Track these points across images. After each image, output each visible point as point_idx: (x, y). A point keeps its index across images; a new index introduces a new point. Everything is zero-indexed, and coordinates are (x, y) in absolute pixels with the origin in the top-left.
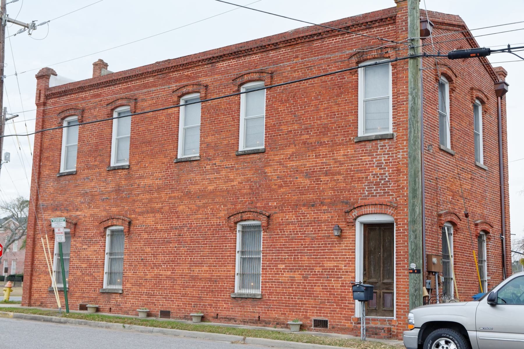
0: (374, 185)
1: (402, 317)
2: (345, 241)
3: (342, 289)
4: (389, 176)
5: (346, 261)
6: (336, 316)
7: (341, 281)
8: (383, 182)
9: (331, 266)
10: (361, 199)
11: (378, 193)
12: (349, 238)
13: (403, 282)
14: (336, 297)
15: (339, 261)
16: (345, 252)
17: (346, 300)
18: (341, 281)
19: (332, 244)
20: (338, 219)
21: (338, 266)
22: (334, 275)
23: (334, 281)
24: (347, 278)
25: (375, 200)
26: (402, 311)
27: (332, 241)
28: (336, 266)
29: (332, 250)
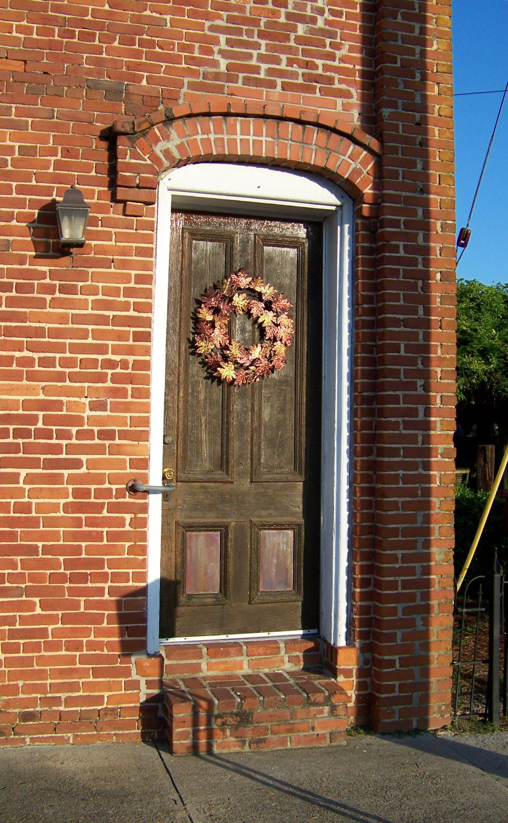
0: (262, 35)
1: (399, 633)
2: (96, 277)
3: (78, 522)
4: (332, 13)
5: (102, 378)
6: (41, 660)
7: (72, 479)
8: (301, 29)
9: (14, 405)
10: (192, 86)
11: (281, 74)
12: (124, 265)
13: (406, 479)
14: (45, 564)
15: (60, 377)
16: (96, 334)
17: (104, 577)
18: (72, 479)
19: (20, 288)
20: (58, 165)
21: (59, 405)
22: (27, 448)
23: (29, 479)
24: (110, 464)
25: (275, 99)
26: (400, 607)
27: (22, 274)
28: (44, 405)
29: (22, 318)
